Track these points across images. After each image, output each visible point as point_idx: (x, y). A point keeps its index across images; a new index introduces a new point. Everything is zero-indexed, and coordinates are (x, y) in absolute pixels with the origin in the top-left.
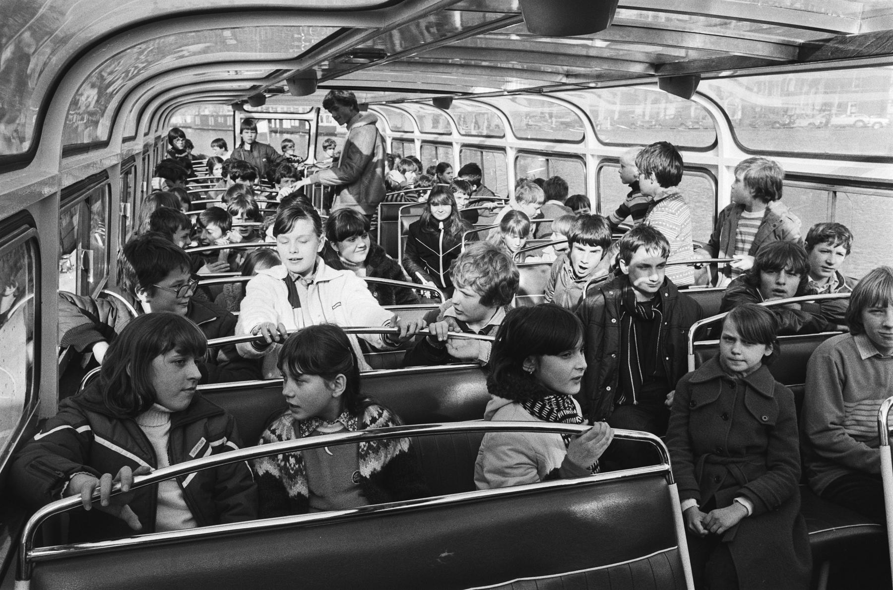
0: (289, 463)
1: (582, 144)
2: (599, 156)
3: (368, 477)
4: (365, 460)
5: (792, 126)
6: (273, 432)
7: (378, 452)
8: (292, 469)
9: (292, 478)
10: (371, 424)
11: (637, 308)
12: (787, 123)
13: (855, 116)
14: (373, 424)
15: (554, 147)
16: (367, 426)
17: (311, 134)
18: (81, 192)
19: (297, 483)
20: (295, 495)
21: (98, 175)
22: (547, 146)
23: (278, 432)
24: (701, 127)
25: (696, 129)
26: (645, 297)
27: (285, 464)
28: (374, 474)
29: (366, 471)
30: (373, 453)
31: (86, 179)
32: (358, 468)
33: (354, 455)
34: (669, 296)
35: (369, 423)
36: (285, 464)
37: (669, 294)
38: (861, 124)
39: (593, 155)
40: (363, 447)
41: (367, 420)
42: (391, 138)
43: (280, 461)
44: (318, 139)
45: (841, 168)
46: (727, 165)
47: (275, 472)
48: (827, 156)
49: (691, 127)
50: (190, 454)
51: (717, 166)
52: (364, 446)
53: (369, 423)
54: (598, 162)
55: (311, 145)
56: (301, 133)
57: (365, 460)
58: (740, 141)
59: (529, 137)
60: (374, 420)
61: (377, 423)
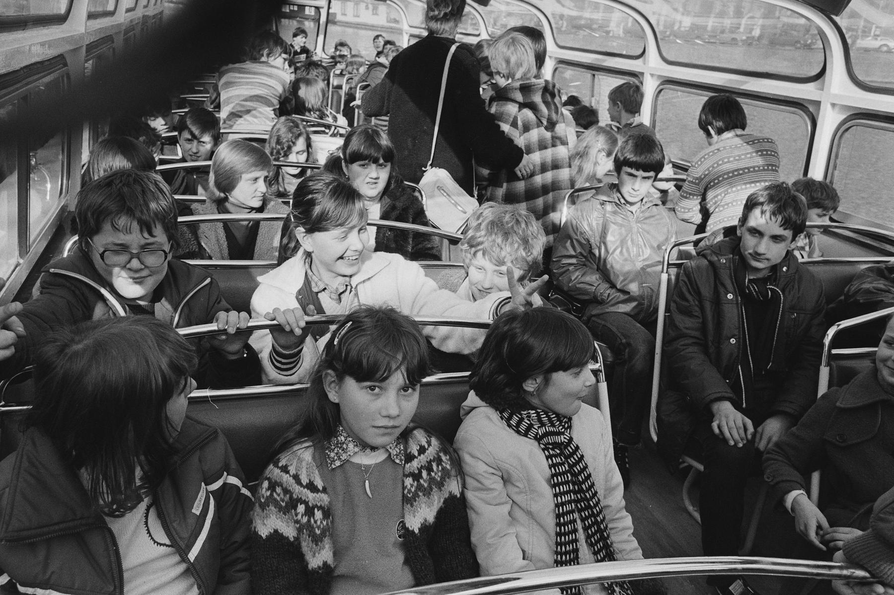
0: (314, 518)
1: (641, 60)
2: (659, 77)
3: (417, 531)
4: (412, 505)
5: (813, 47)
6: (285, 469)
7: (430, 494)
8: (319, 527)
9: (317, 540)
10: (419, 455)
11: (748, 288)
12: (808, 43)
13: (881, 40)
14: (422, 455)
15: (604, 61)
16: (414, 457)
17: (321, 22)
18: (16, 86)
19: (324, 548)
20: (319, 567)
21: (47, 63)
22: (730, 80)
23: (292, 470)
24: (718, 41)
25: (712, 43)
26: (14, 174)
27: (309, 521)
28: (424, 528)
29: (414, 523)
30: (424, 495)
31: (22, 69)
32: (403, 517)
33: (400, 498)
34: (787, 271)
35: (416, 454)
36: (309, 521)
37: (788, 268)
38: (885, 49)
39: (833, 105)
40: (409, 487)
41: (414, 450)
42: (409, 35)
43: (299, 517)
44: (328, 27)
45: (596, 59)
46: (652, 73)
47: (289, 531)
48: (876, 89)
49: (707, 41)
50: (194, 511)
51: (820, 102)
52: (412, 486)
53: (416, 454)
54: (658, 83)
55: (319, 34)
56: (298, 19)
57: (412, 505)
58: (860, 78)
59: (624, 53)
60: (422, 450)
61: (426, 454)
